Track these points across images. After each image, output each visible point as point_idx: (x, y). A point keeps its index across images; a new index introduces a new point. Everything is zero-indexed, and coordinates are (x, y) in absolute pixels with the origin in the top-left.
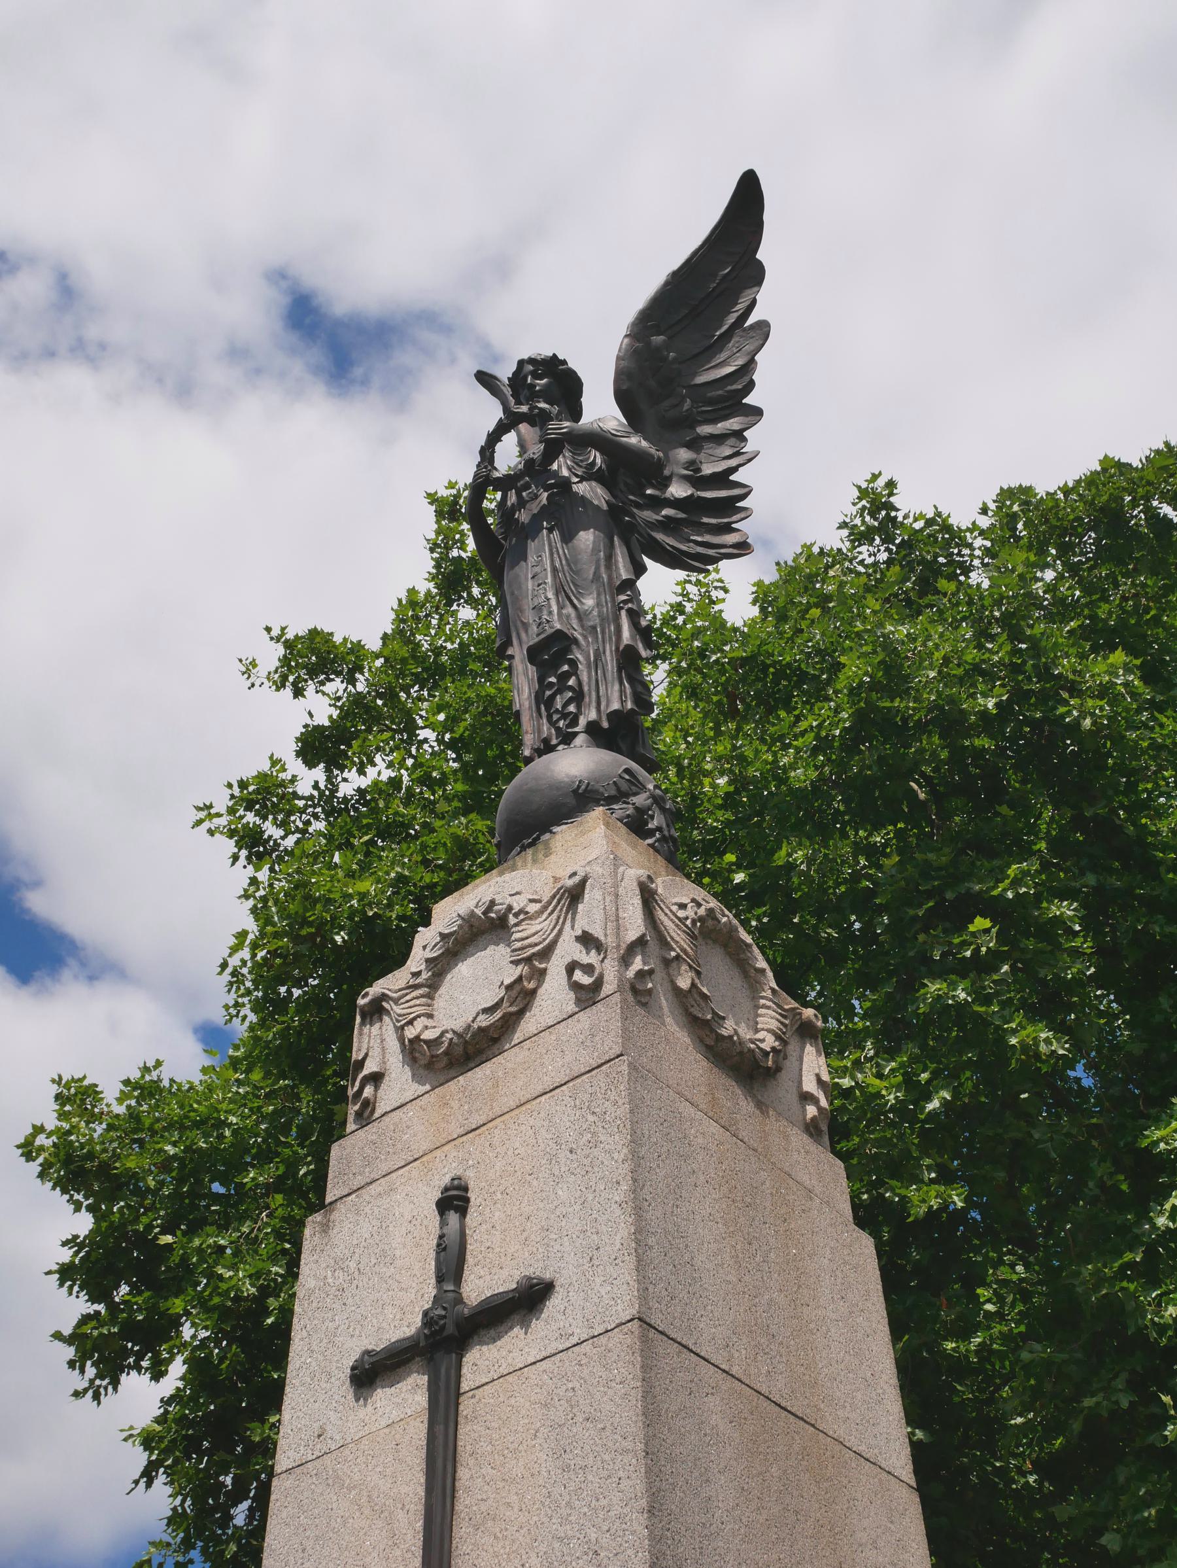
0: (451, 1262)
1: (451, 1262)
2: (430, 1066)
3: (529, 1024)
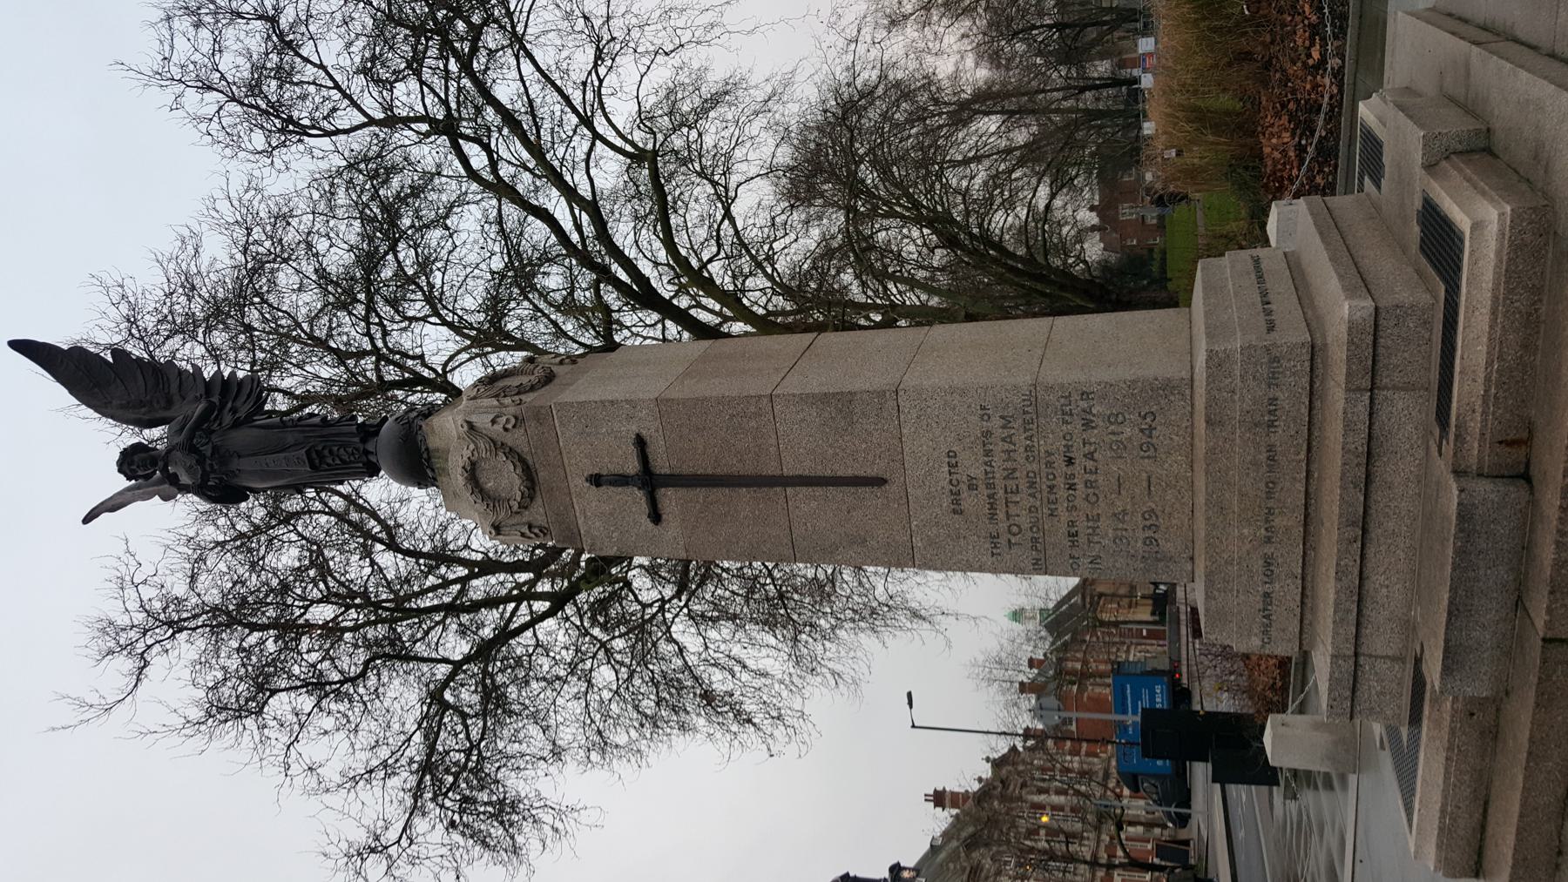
0: (621, 480)
1: (621, 480)
2: (532, 498)
3: (523, 448)
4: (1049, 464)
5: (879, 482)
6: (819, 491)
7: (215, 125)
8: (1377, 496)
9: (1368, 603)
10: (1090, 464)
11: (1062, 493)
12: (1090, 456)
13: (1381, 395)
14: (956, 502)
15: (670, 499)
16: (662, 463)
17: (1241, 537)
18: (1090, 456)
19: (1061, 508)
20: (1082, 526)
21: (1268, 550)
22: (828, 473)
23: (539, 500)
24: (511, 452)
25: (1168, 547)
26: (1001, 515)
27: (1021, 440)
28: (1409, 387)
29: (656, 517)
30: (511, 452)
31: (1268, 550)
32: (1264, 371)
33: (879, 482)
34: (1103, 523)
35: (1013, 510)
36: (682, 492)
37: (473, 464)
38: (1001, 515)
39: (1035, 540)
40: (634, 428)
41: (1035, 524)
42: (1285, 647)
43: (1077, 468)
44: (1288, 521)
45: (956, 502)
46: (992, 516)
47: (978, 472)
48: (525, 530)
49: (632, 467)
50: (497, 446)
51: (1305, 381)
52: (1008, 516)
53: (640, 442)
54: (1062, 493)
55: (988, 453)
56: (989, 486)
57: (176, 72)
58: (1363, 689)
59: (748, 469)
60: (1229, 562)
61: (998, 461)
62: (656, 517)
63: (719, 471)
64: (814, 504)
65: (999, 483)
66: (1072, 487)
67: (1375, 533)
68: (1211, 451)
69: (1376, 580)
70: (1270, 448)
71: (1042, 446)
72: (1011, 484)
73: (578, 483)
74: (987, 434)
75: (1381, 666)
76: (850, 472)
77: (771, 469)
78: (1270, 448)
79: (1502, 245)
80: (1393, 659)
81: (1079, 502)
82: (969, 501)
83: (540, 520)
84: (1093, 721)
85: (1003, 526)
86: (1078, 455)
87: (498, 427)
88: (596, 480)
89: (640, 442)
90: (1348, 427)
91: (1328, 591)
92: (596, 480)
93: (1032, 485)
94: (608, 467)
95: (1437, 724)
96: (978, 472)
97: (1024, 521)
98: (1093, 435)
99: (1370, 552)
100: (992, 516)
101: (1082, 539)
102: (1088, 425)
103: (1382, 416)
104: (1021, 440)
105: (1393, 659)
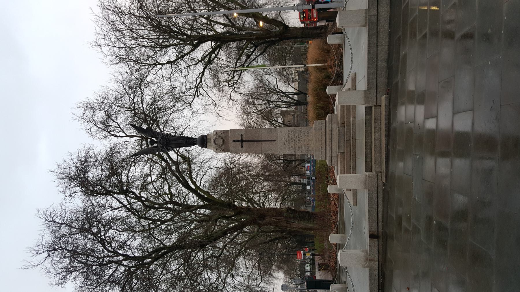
1: (238, 141)
5: (274, 141)
7: (89, 131)
15: (244, 143)
29: (242, 147)
33: (274, 141)
44: (324, 142)
49: (240, 139)
50: (220, 136)
53: (242, 135)
57: (85, 117)
62: (242, 147)
69: (333, 146)
71: (296, 135)
73: (231, 141)
82: (286, 143)
84: (312, 67)
88: (234, 141)
89: (242, 135)
91: (328, 140)
92: (234, 141)
94: (236, 139)
97: (293, 146)
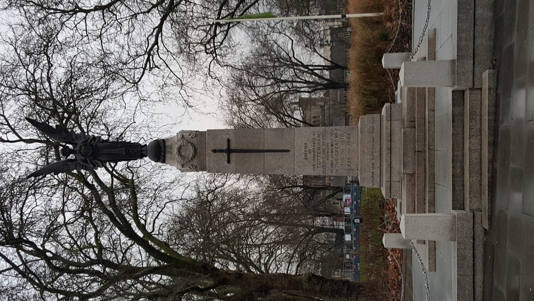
0: (221, 151)
1: (221, 151)
2: (195, 157)
4: (328, 146)
5: (288, 151)
6: (273, 153)
8: (393, 143)
9: (392, 169)
10: (336, 146)
11: (330, 153)
12: (336, 144)
13: (392, 122)
14: (306, 156)
16: (233, 147)
17: (368, 158)
18: (336, 144)
19: (330, 157)
20: (334, 161)
21: (373, 161)
22: (276, 149)
23: (196, 158)
24: (192, 144)
25: (353, 167)
26: (316, 159)
27: (322, 140)
28: (397, 120)
29: (229, 162)
30: (192, 144)
31: (373, 161)
32: (371, 120)
33: (288, 151)
34: (339, 161)
35: (319, 158)
36: (237, 154)
37: (180, 147)
38: (316, 159)
39: (323, 166)
40: (228, 137)
41: (324, 162)
42: (376, 186)
43: (334, 147)
44: (377, 154)
45: (306, 156)
46: (314, 160)
47: (311, 148)
48: (191, 166)
51: (379, 123)
52: (318, 160)
53: (229, 140)
54: (330, 153)
55: (314, 143)
56: (314, 152)
58: (392, 189)
59: (255, 148)
60: (365, 165)
61: (316, 145)
62: (229, 162)
63: (248, 149)
64: (271, 157)
65: (316, 151)
66: (332, 152)
67: (393, 152)
68: (361, 138)
69: (393, 163)
70: (373, 137)
72: (319, 151)
74: (314, 139)
75: (396, 184)
76: (281, 149)
77: (261, 148)
78: (373, 137)
79: (413, 99)
80: (398, 182)
81: (334, 156)
82: (310, 156)
83: (195, 164)
85: (316, 162)
86: (334, 144)
87: (190, 137)
88: (215, 151)
89: (229, 140)
90: (387, 128)
92: (215, 151)
93: (323, 151)
95: (404, 184)
96: (311, 148)
97: (321, 161)
98: (337, 139)
99: (392, 156)
100: (314, 160)
101: (334, 165)
102: (336, 137)
103: (393, 126)
104: (322, 140)
105: (398, 182)
